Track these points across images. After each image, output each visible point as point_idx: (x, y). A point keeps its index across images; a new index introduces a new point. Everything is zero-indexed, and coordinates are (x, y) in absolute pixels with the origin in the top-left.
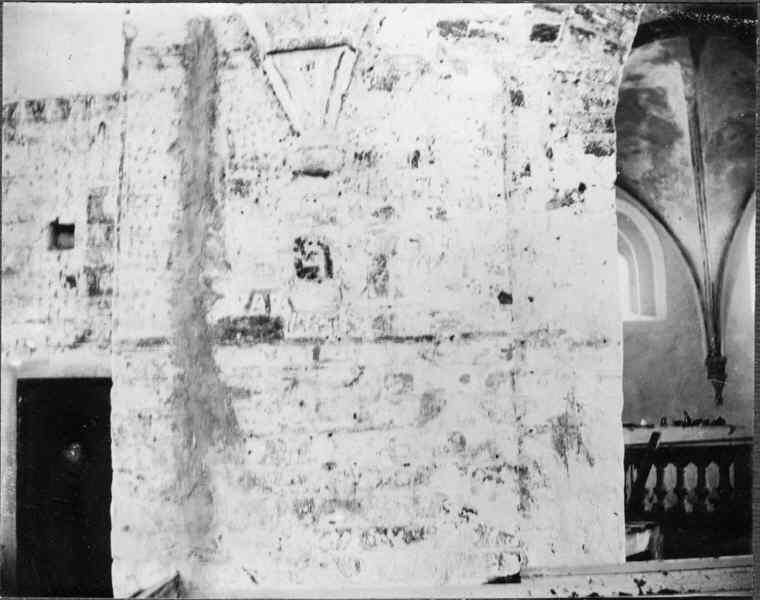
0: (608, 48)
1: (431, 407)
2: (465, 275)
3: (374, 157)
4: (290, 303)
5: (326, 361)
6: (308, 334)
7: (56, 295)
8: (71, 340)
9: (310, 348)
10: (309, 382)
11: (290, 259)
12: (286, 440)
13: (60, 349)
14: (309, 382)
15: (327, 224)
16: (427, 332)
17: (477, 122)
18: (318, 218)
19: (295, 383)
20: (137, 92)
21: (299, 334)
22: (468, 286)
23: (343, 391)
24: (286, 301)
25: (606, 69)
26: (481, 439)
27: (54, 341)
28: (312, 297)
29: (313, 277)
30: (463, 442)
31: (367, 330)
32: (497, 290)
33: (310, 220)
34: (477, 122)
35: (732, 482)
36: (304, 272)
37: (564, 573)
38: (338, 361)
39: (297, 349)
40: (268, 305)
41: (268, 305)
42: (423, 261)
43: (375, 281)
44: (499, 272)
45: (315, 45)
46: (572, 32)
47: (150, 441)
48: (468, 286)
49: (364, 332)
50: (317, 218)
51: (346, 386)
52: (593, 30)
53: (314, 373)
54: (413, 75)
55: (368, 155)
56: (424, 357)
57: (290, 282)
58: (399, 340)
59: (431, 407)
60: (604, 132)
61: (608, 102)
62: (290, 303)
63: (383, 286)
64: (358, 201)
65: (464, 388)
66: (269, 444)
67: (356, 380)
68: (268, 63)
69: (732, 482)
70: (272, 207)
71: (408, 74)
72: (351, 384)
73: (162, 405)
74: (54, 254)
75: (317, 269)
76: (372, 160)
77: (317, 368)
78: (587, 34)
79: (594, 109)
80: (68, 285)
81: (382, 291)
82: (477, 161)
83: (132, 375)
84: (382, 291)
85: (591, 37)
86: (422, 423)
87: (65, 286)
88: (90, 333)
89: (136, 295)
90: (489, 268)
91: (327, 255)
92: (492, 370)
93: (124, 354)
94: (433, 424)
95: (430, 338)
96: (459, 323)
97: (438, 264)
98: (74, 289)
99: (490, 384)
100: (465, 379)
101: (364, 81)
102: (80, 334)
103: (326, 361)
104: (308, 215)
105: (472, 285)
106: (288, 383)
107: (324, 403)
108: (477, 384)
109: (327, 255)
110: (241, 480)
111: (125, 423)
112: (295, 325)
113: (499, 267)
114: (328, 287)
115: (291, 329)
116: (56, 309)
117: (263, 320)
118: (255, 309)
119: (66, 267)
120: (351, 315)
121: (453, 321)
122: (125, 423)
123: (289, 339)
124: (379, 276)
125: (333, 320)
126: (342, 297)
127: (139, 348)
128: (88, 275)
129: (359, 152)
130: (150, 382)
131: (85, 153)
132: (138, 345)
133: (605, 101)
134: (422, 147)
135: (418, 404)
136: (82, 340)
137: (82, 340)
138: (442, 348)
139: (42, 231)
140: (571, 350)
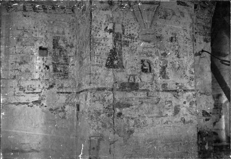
1: (177, 111)
5: (150, 96)
11: (140, 66)
12: (140, 120)
21: (143, 88)
22: (185, 77)
23: (155, 105)
26: (189, 119)
28: (146, 78)
31: (160, 88)
33: (145, 55)
36: (144, 70)
40: (134, 80)
45: (37, 2)
46: (201, 7)
48: (185, 77)
49: (159, 89)
50: (147, 54)
52: (205, 7)
54: (171, 15)
55: (160, 37)
56: (174, 96)
60: (208, 36)
61: (209, 28)
67: (158, 102)
71: (170, 15)
72: (157, 103)
73: (105, 109)
78: (204, 8)
80: (46, 68)
83: (95, 99)
85: (205, 8)
87: (45, 68)
91: (150, 65)
94: (177, 115)
97: (178, 70)
100: (185, 103)
101: (159, 15)
103: (150, 96)
106: (140, 103)
107: (80, 103)
108: (188, 104)
109: (150, 65)
114: (150, 76)
116: (42, 76)
117: (133, 84)
118: (131, 80)
124: (163, 73)
130: (101, 102)
132: (97, 90)
133: (208, 27)
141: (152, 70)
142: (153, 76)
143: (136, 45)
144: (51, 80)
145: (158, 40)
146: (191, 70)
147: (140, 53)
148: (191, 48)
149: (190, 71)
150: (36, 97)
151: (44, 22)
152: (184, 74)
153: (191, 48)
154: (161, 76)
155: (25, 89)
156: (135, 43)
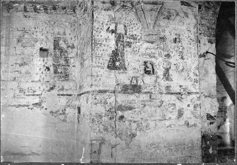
0: (213, 13)
1: (180, 114)
2: (188, 76)
5: (153, 99)
8: (49, 88)
9: (149, 95)
10: (148, 105)
14: (148, 105)
19: (145, 106)
21: (145, 91)
22: (189, 79)
25: (213, 19)
28: (149, 79)
29: (149, 74)
30: (188, 124)
35: (84, 148)
36: (147, 72)
38: (156, 99)
39: (144, 95)
41: (137, 82)
44: (197, 75)
51: (159, 107)
53: (150, 103)
54: (175, 16)
56: (178, 99)
57: (143, 75)
58: (172, 94)
59: (180, 114)
61: (214, 28)
62: (143, 81)
65: (189, 108)
66: (138, 125)
69: (84, 148)
75: (150, 71)
77: (150, 101)
78: (208, 8)
79: (210, 30)
80: (47, 70)
82: (191, 43)
86: (178, 118)
87: (45, 70)
89: (98, 76)
91: (153, 67)
92: (195, 103)
93: (94, 95)
94: (181, 118)
95: (180, 93)
98: (49, 71)
99: (194, 107)
100: (189, 106)
102: (51, 86)
103: (153, 99)
109: (153, 67)
110: (130, 135)
111: (94, 117)
112: (145, 88)
114: (153, 77)
115: (143, 89)
117: (135, 86)
120: (160, 86)
122: (94, 117)
123: (143, 92)
127: (99, 93)
128: (54, 67)
132: (99, 92)
135: (177, 113)
137: (52, 89)
138: (183, 96)
140: (205, 98)
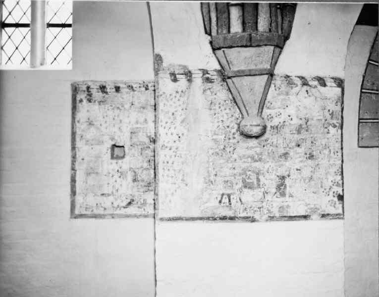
3: (280, 128)
4: (240, 200)
6: (249, 215)
7: (116, 181)
13: (119, 209)
15: (257, 161)
16: (303, 214)
17: (329, 110)
18: (253, 158)
20: (164, 93)
24: (238, 199)
27: (115, 205)
32: (336, 194)
33: (249, 159)
34: (329, 110)
36: (247, 186)
37: (261, 44)
42: (302, 180)
43: (280, 189)
47: (105, 114)
50: (252, 158)
62: (240, 200)
63: (283, 192)
64: (272, 150)
68: (229, 81)
70: (232, 153)
74: (114, 161)
76: (279, 129)
81: (283, 194)
84: (283, 194)
88: (133, 201)
90: (333, 183)
96: (319, 209)
102: (129, 201)
104: (249, 157)
105: (325, 191)
113: (338, 183)
114: (258, 193)
119: (121, 168)
121: (316, 208)
125: (260, 208)
126: (264, 197)
129: (273, 125)
131: (128, 111)
134: (327, 196)
136: (130, 203)
139: (108, 150)
141: (261, 183)
142: (264, 194)
143: (234, 144)
144: (54, 282)
145: (273, 132)
146: (335, 180)
147: (240, 157)
148: (337, 140)
149: (333, 181)
150: (163, 139)
151: (88, 91)
152: (322, 187)
153: (337, 140)
154: (278, 193)
155: (94, 208)
156: (231, 141)
